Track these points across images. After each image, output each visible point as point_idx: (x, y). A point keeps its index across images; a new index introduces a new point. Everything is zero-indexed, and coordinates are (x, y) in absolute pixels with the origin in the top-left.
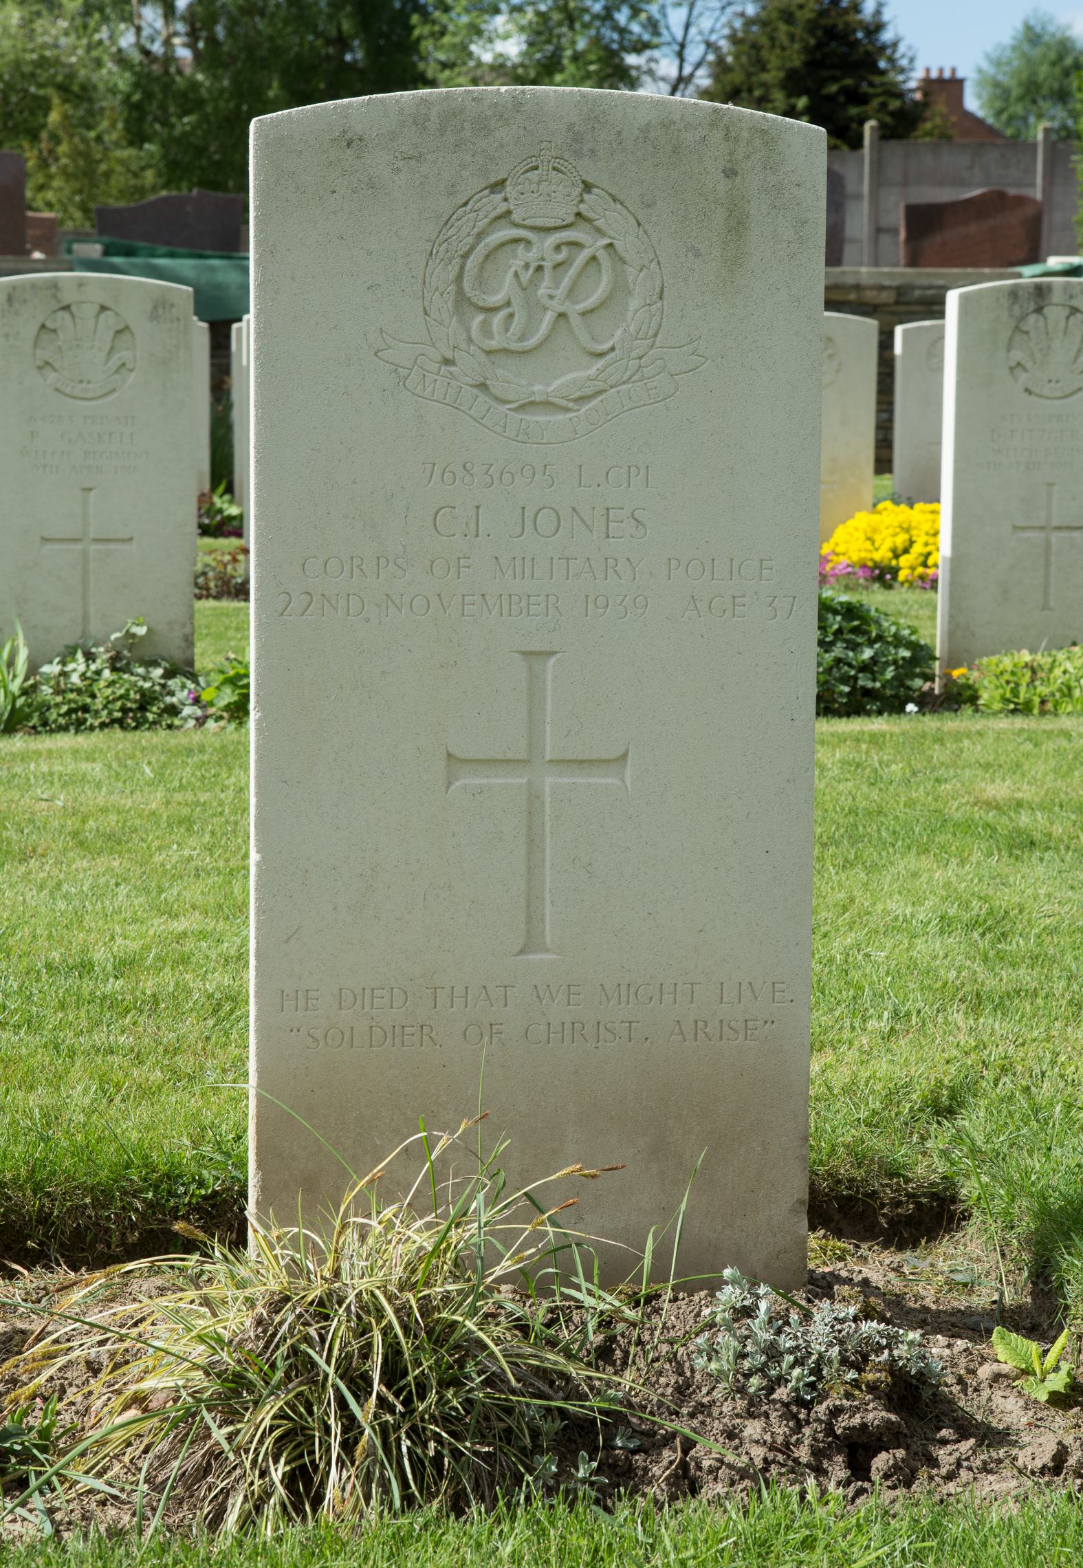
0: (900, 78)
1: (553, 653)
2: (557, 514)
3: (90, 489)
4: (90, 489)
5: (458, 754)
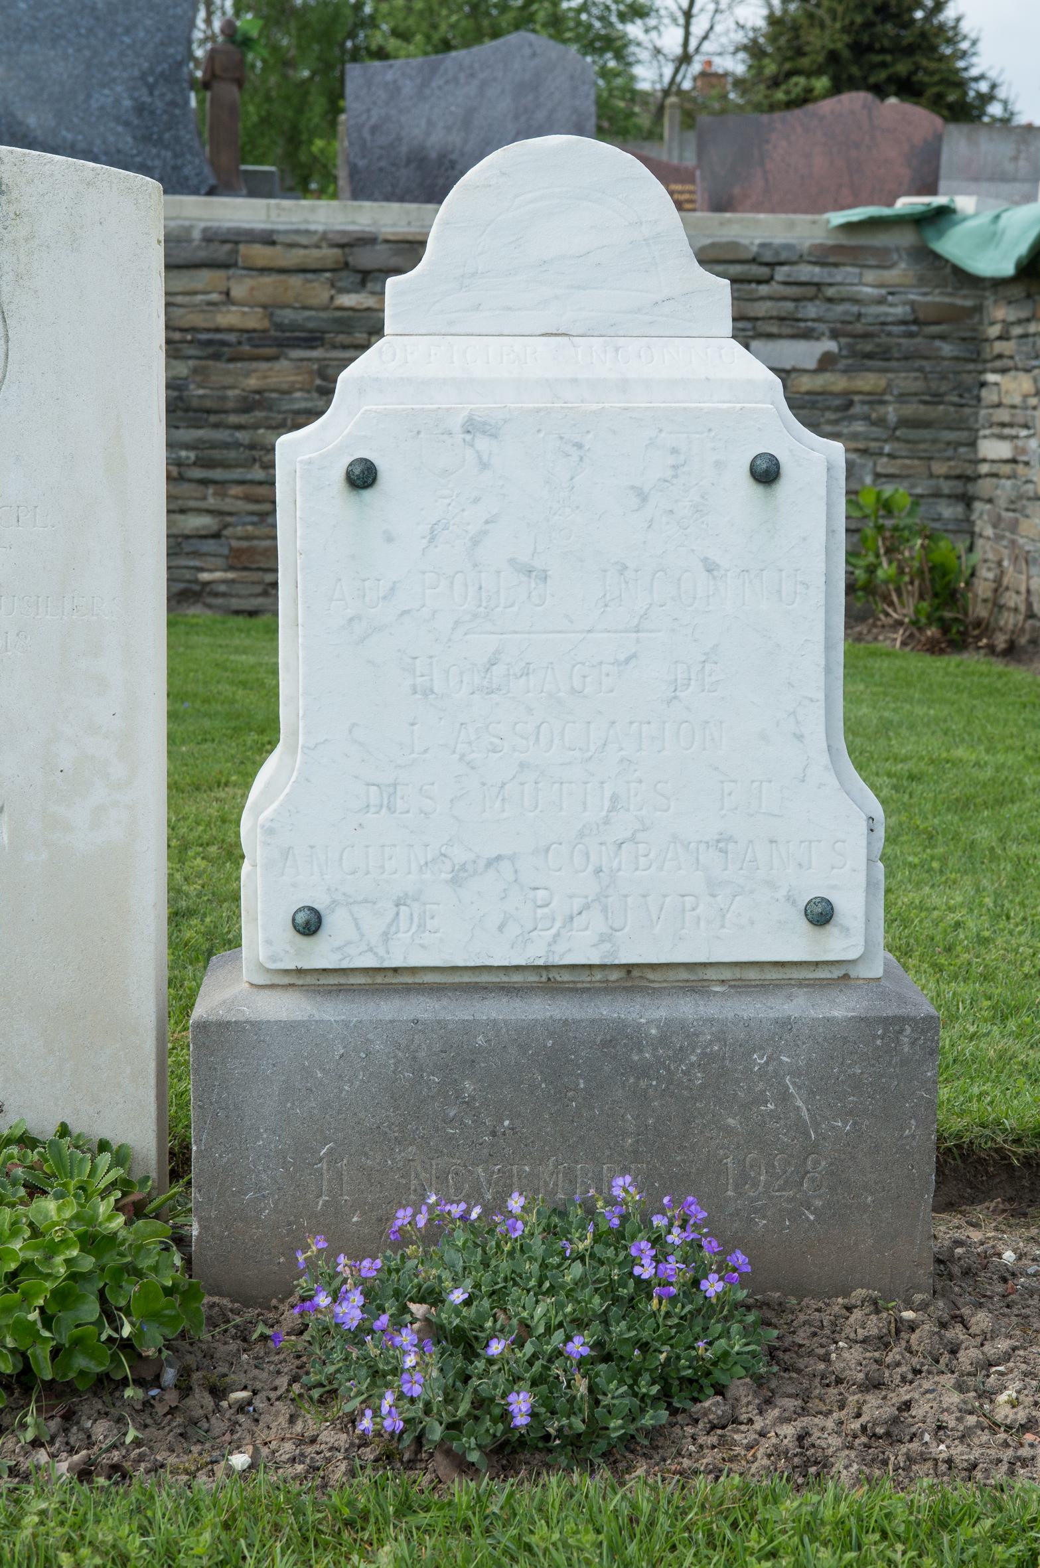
0: (961, 64)
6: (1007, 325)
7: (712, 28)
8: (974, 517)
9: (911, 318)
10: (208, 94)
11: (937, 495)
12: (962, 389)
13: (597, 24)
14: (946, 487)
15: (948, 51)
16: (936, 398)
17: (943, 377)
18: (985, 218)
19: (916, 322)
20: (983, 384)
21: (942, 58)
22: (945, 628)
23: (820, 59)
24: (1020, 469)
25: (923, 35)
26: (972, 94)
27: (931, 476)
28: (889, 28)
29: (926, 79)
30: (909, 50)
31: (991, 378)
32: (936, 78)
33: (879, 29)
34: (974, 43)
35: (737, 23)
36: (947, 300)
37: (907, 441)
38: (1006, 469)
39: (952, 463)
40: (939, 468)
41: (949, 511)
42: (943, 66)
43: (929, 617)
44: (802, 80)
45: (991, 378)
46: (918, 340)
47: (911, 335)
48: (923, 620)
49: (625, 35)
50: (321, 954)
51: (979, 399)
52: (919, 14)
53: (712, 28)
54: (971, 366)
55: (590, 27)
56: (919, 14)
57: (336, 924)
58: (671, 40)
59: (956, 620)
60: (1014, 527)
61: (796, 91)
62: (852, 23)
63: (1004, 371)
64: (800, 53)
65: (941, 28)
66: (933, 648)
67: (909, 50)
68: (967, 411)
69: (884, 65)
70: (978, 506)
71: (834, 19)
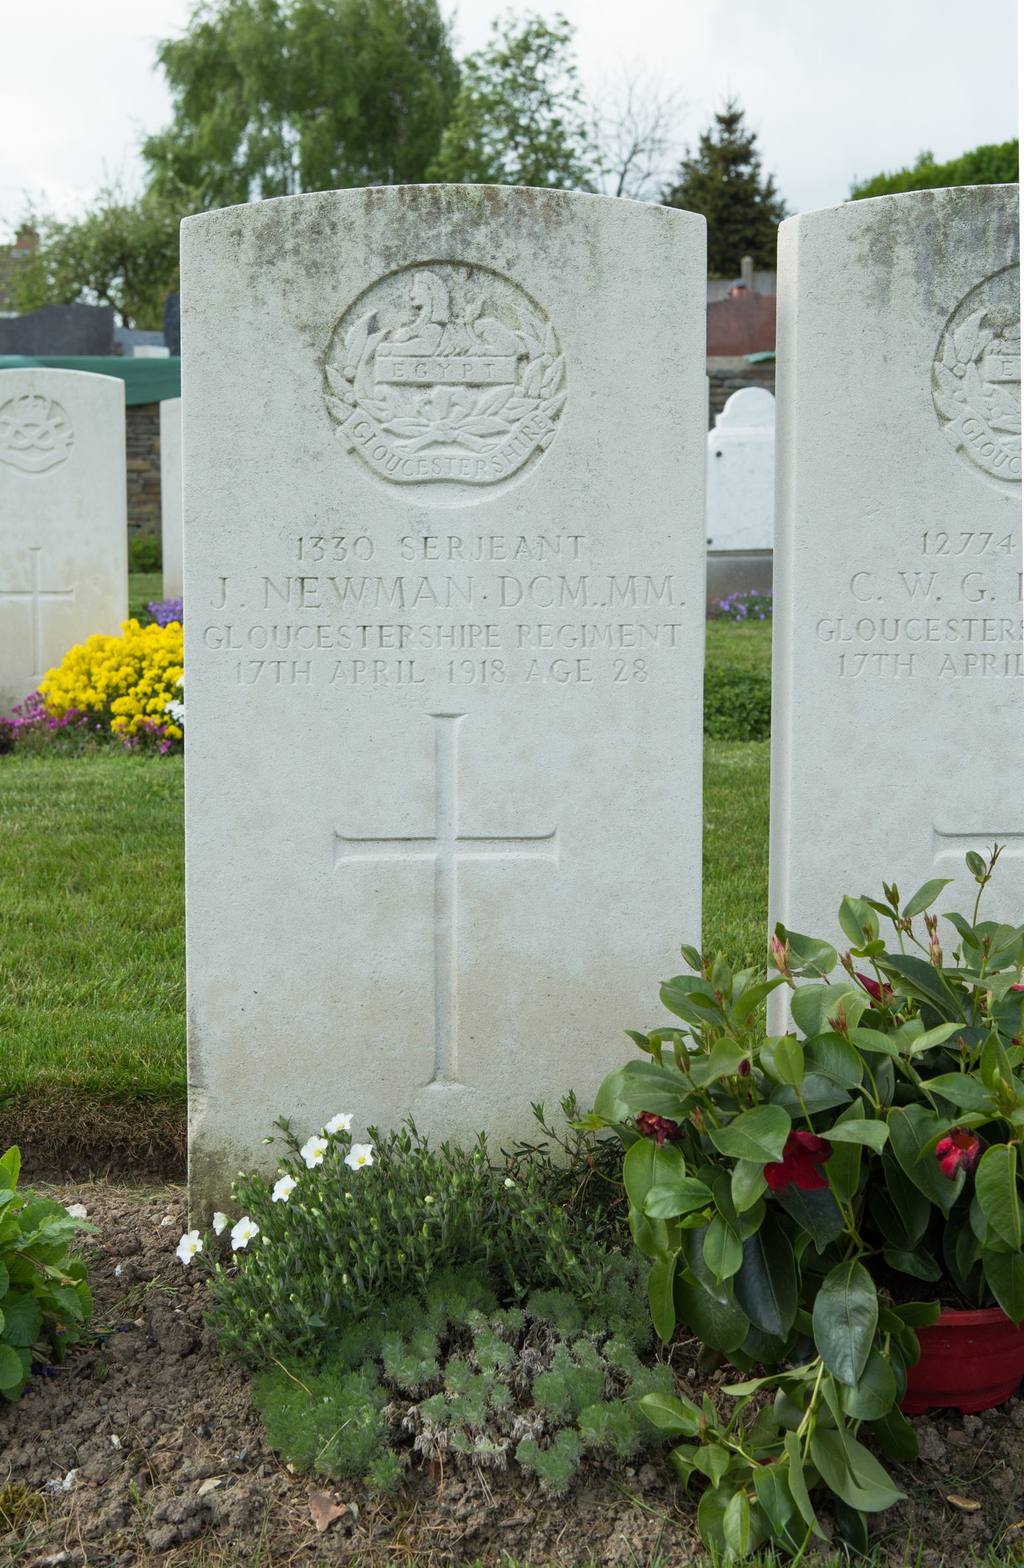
28: (739, 209)
30: (753, 221)
33: (733, 210)
35: (577, 91)
50: (712, 548)
52: (757, 199)
57: (715, 542)
67: (753, 221)
69: (737, 231)
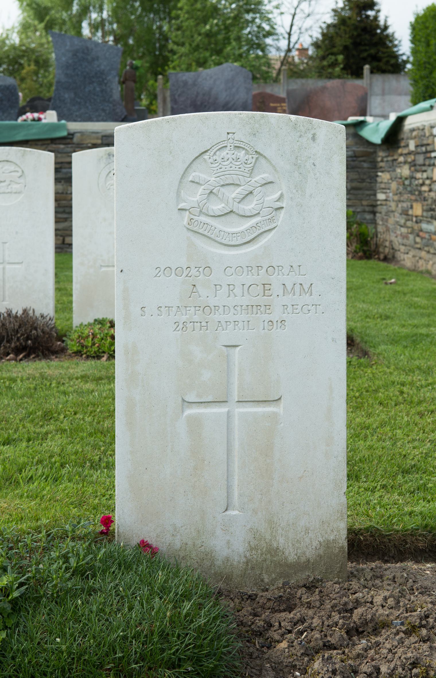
0: (395, 49)
1: (237, 346)
2: (248, 289)
3: (6, 243)
4: (6, 243)
5: (187, 400)
6: (383, 158)
7: (299, 39)
8: (377, 218)
9: (353, 155)
10: (124, 86)
11: (364, 211)
12: (371, 178)
13: (254, 38)
14: (367, 209)
15: (390, 45)
16: (363, 181)
17: (365, 174)
18: (374, 125)
19: (355, 156)
20: (377, 176)
21: (388, 47)
22: (365, 252)
23: (341, 48)
24: (388, 203)
25: (381, 39)
26: (400, 60)
27: (362, 205)
28: (367, 37)
29: (382, 55)
30: (375, 45)
31: (379, 174)
32: (386, 55)
34: (400, 41)
36: (365, 150)
37: (354, 194)
38: (384, 203)
39: (369, 201)
40: (365, 203)
41: (368, 217)
42: (388, 50)
43: (360, 249)
44: (333, 58)
45: (379, 174)
46: (356, 163)
47: (354, 161)
48: (358, 250)
49: (265, 43)
51: (376, 180)
53: (299, 39)
54: (373, 170)
55: (252, 40)
56: (379, 31)
58: (283, 44)
59: (368, 250)
60: (387, 221)
61: (331, 61)
62: (353, 35)
63: (382, 172)
64: (334, 46)
65: (387, 36)
66: (361, 258)
68: (373, 184)
70: (378, 215)
71: (346, 33)
